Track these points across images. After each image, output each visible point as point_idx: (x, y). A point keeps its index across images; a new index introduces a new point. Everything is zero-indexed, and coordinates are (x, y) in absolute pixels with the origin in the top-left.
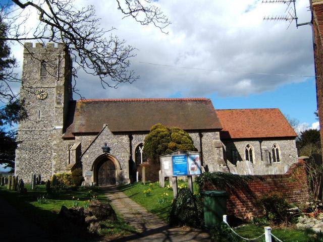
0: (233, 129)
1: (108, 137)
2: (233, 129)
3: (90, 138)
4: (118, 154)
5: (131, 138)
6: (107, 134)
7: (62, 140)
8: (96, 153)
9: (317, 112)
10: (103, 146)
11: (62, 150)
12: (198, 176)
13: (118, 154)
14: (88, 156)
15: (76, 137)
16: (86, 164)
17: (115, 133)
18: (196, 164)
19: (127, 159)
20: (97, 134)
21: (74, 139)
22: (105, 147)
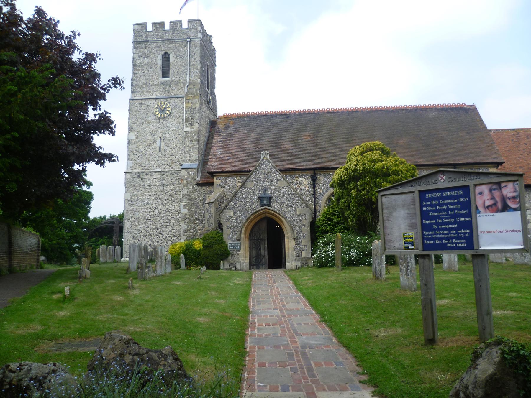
0: (521, 167)
1: (270, 177)
2: (521, 167)
3: (238, 181)
4: (289, 209)
5: (314, 180)
6: (267, 171)
7: (196, 187)
8: (248, 206)
9: (100, 164)
10: (260, 193)
11: (197, 205)
12: (453, 268)
13: (289, 209)
14: (232, 214)
15: (216, 181)
16: (229, 227)
17: (283, 171)
18: (156, 352)
19: (307, 220)
20: (246, 173)
21: (212, 184)
22: (263, 196)
